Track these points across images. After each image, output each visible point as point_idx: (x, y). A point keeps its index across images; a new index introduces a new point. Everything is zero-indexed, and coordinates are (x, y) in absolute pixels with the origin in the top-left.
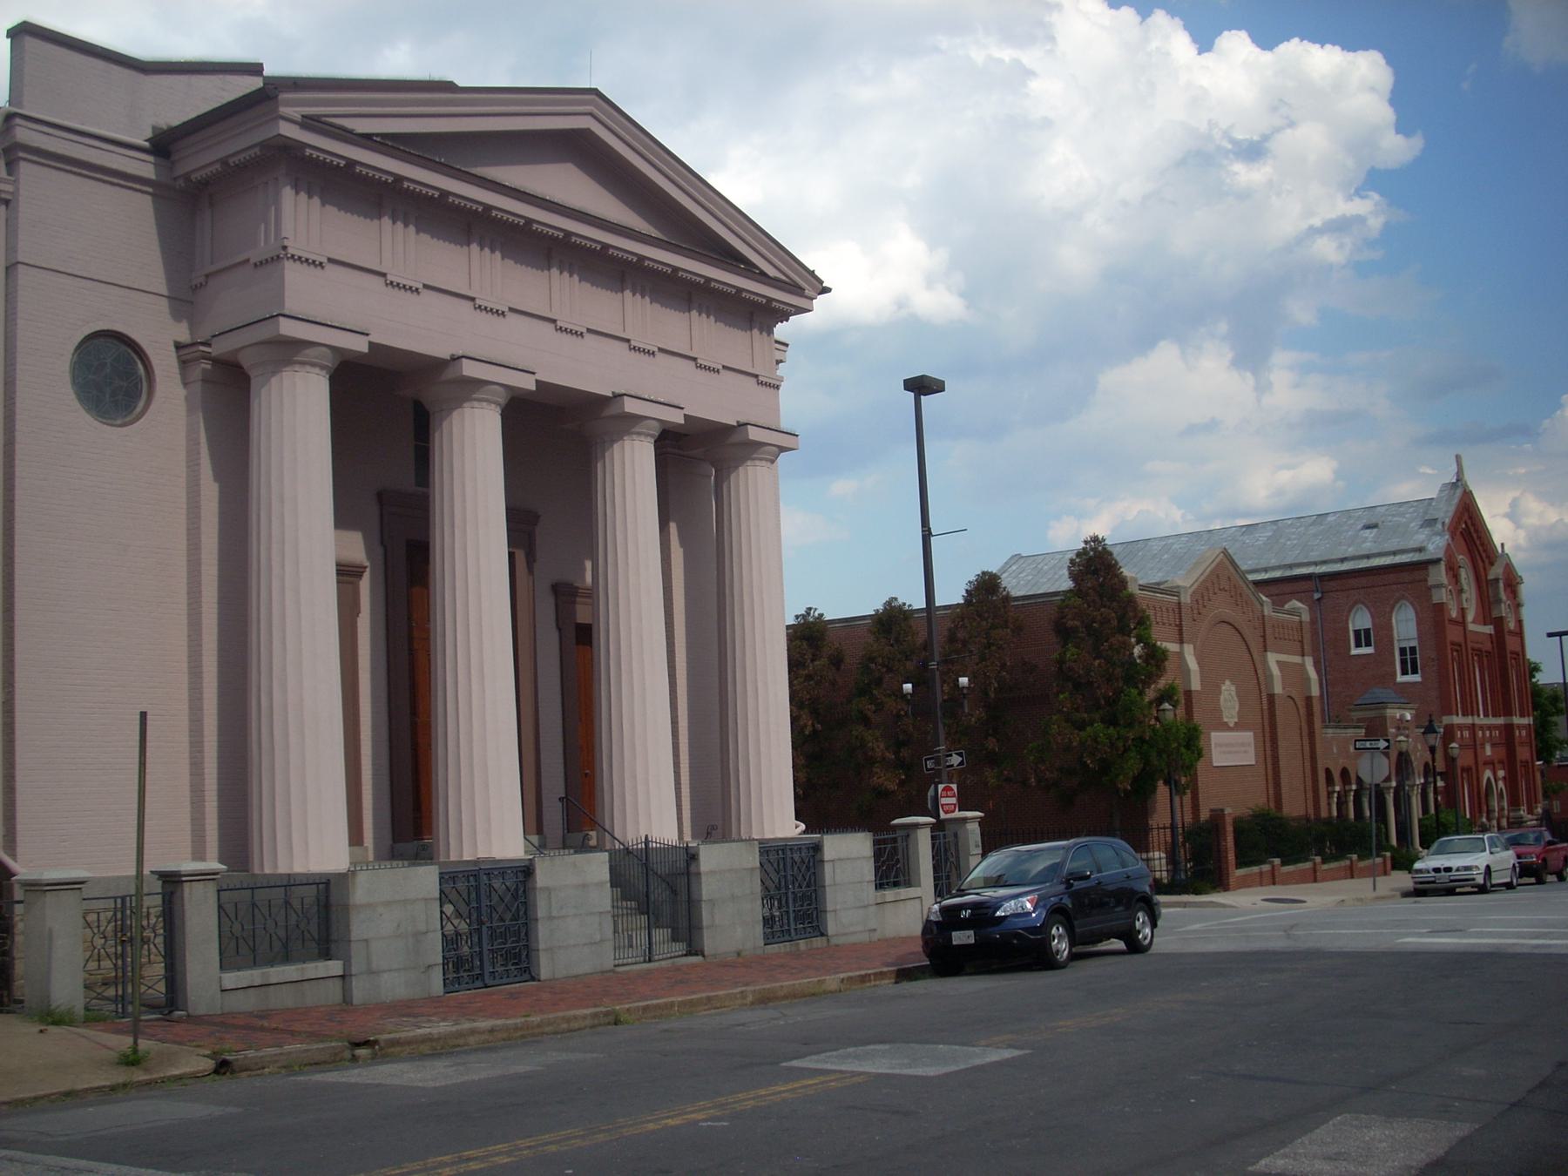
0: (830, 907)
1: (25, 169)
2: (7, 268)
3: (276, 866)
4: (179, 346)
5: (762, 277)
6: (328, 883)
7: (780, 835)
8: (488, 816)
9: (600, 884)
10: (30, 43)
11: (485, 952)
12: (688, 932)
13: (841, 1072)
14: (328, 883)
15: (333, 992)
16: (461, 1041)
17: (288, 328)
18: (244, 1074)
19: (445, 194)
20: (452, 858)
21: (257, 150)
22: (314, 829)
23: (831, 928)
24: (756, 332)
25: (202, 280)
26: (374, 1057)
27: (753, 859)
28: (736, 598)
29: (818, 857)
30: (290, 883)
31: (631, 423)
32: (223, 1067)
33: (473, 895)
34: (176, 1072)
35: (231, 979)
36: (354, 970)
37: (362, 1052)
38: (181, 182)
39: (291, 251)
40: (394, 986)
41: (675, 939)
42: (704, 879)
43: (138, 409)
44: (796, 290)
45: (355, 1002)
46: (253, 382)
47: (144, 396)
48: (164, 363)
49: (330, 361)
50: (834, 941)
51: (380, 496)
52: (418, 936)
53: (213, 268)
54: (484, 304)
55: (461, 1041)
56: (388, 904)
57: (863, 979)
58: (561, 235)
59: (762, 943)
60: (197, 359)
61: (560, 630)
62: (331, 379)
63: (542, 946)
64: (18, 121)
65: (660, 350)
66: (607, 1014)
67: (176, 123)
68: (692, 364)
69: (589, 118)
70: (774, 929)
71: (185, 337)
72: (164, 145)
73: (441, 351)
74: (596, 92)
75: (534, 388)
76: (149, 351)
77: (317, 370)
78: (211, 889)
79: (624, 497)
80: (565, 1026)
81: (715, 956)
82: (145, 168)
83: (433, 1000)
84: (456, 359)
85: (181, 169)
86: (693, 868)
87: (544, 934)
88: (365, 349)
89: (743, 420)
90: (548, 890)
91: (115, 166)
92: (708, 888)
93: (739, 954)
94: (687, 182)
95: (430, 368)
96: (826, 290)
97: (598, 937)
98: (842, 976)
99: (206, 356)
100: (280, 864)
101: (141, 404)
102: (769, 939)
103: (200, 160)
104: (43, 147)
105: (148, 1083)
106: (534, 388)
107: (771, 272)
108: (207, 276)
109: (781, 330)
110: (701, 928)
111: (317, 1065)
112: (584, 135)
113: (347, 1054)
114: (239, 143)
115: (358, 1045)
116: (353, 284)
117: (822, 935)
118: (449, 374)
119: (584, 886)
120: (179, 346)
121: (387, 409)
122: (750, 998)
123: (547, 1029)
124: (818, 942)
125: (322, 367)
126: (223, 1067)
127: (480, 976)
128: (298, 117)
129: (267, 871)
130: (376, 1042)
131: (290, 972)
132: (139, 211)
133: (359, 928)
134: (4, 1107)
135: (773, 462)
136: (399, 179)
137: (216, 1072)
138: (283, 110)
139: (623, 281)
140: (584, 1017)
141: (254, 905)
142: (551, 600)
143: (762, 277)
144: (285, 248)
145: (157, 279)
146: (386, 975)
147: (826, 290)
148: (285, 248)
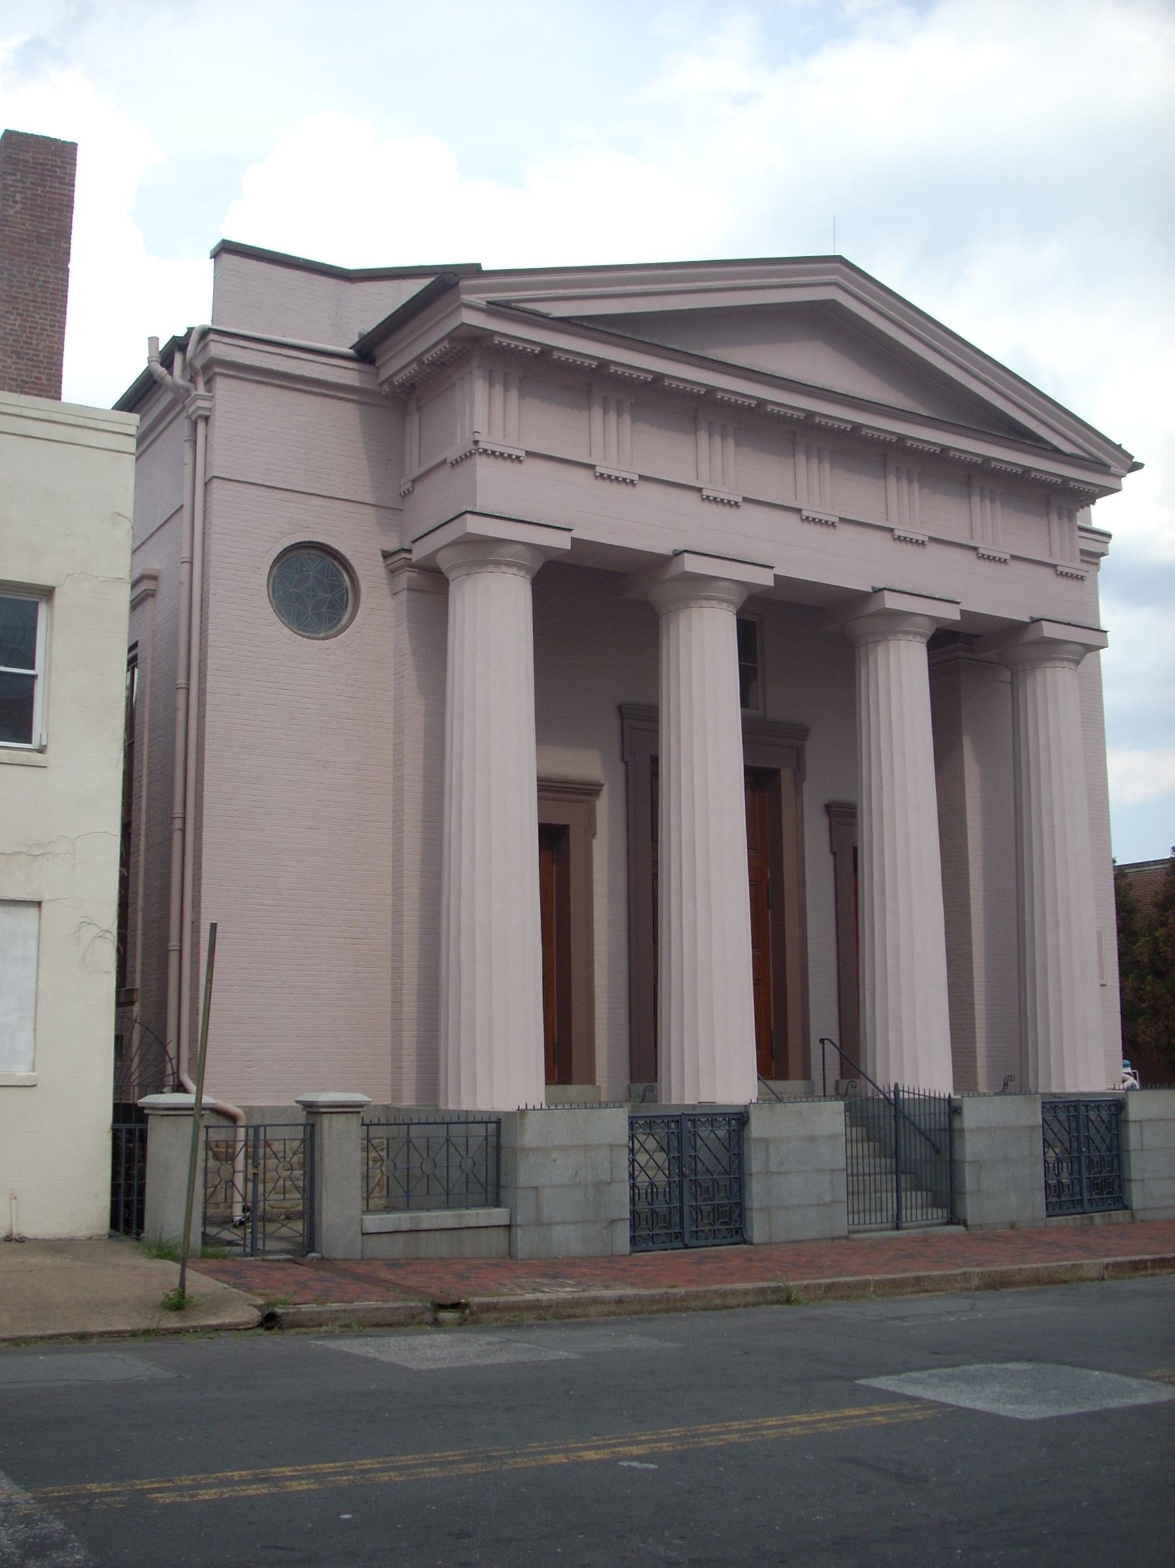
0: (1135, 1174)
1: (220, 384)
2: (206, 484)
3: (459, 1103)
4: (386, 555)
5: (1055, 453)
6: (498, 1123)
7: (1084, 1089)
8: (715, 1056)
9: (832, 1138)
10: (226, 258)
11: (686, 1209)
12: (948, 1198)
13: (913, 1399)
14: (498, 1123)
15: (497, 1240)
16: (579, 1311)
17: (476, 526)
18: (293, 1331)
19: (945, 449)
20: (674, 1102)
21: (446, 343)
22: (500, 1065)
23: (1137, 1199)
24: (1054, 518)
25: (409, 485)
26: (462, 1323)
27: (1033, 1116)
28: (1034, 814)
29: (1122, 1116)
30: (467, 1120)
31: (699, 586)
32: (270, 1321)
33: (1075, 1145)
34: (214, 1321)
35: (373, 1222)
36: (519, 1220)
37: (447, 1316)
38: (386, 387)
39: (482, 445)
40: (567, 1239)
41: (935, 1205)
42: (967, 1135)
43: (343, 622)
44: (1101, 467)
45: (520, 1254)
46: (451, 587)
47: (350, 608)
48: (369, 571)
49: (739, 597)
50: (1140, 1216)
51: (621, 710)
52: (600, 1186)
53: (417, 472)
54: (712, 494)
55: (579, 1311)
56: (563, 1148)
57: (1136, 1266)
58: (1060, 481)
59: (1044, 1214)
60: (402, 567)
61: (834, 854)
62: (738, 614)
63: (756, 1205)
64: (212, 336)
65: (842, 520)
66: (776, 1290)
67: (370, 329)
68: (888, 536)
69: (833, 288)
70: (1060, 1198)
71: (392, 546)
72: (367, 351)
73: (661, 546)
74: (839, 259)
75: (958, 618)
76: (354, 562)
77: (514, 570)
78: (187, 1124)
79: (889, 703)
80: (718, 1301)
81: (981, 1226)
82: (348, 375)
83: (612, 1258)
84: (878, 591)
85: (385, 374)
86: (956, 1125)
87: (757, 1192)
88: (771, 583)
89: (1037, 615)
90: (766, 1142)
91: (315, 375)
92: (971, 1148)
93: (1012, 1226)
94: (951, 347)
95: (654, 566)
96: (1137, 466)
97: (828, 1198)
98: (1106, 1260)
99: (410, 565)
100: (686, 1097)
101: (346, 617)
102: (1052, 1209)
103: (400, 361)
104: (239, 360)
105: (177, 1332)
106: (958, 618)
107: (1067, 448)
108: (414, 481)
109: (1102, 514)
110: (963, 1193)
111: (384, 1325)
112: (830, 306)
113: (428, 1317)
114: (427, 340)
115: (442, 1307)
116: (549, 477)
117: (1126, 1208)
118: (1031, 635)
119: (812, 1138)
120: (386, 555)
121: (597, 613)
122: (975, 1282)
123: (693, 1304)
124: (1118, 1216)
125: (520, 567)
126: (270, 1321)
127: (680, 1235)
128: (482, 303)
129: (451, 1107)
130: (467, 1305)
131: (446, 1217)
132: (343, 420)
133: (526, 1173)
134: (2, 1345)
135: (1077, 663)
136: (810, 415)
137: (260, 1325)
138: (466, 298)
139: (884, 464)
140: (745, 1293)
141: (408, 1141)
142: (824, 823)
143: (1055, 453)
144: (476, 442)
145: (360, 484)
146: (558, 1229)
147: (1137, 466)
148: (476, 442)
